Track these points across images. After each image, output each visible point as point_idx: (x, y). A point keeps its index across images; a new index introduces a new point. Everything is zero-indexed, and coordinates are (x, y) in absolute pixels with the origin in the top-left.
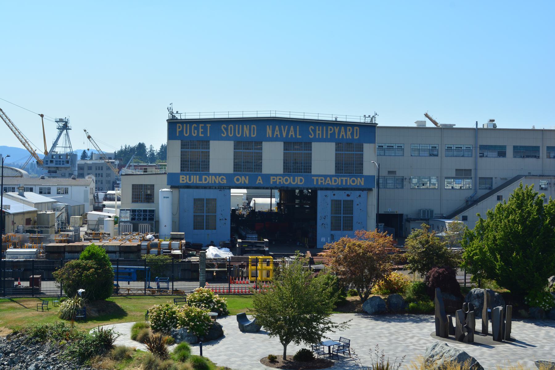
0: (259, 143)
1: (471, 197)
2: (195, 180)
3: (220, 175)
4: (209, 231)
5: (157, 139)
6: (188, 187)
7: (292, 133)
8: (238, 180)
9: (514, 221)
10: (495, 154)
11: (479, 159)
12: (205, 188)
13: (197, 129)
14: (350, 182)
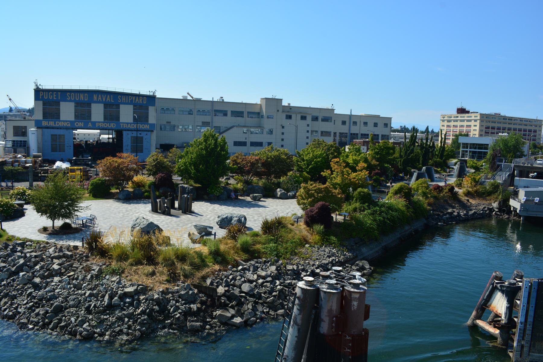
0: (89, 105)
2: (52, 124)
3: (66, 121)
4: (61, 153)
6: (47, 128)
7: (108, 99)
8: (77, 124)
9: (202, 149)
10: (222, 114)
11: (214, 117)
12: (58, 128)
13: (52, 95)
14: (141, 126)
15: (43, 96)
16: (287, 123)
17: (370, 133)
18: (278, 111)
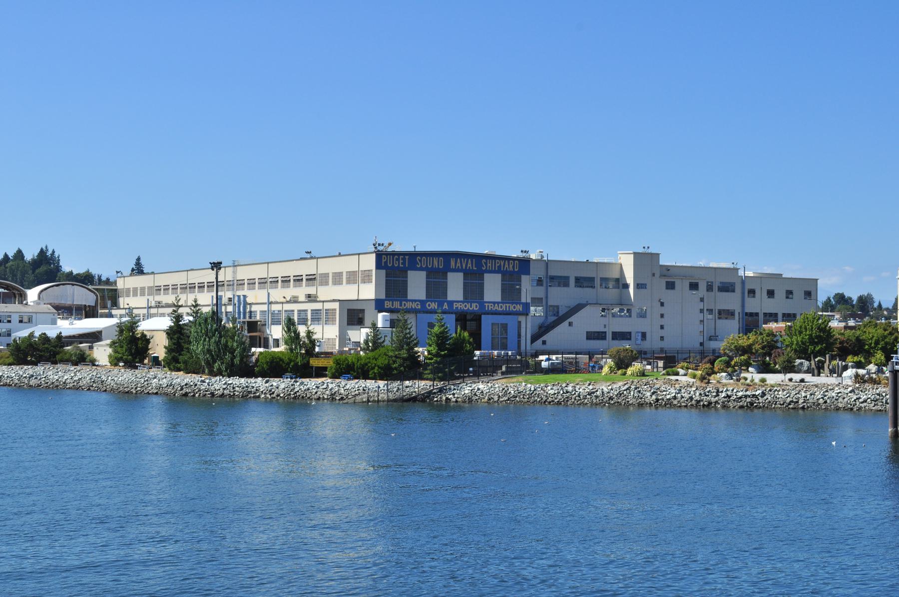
1: (543, 323)
2: (397, 305)
3: (415, 301)
5: (855, 298)
13: (398, 260)
15: (386, 263)
16: (669, 296)
17: (798, 312)
18: (654, 275)
